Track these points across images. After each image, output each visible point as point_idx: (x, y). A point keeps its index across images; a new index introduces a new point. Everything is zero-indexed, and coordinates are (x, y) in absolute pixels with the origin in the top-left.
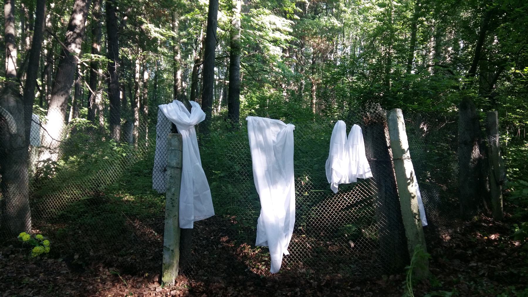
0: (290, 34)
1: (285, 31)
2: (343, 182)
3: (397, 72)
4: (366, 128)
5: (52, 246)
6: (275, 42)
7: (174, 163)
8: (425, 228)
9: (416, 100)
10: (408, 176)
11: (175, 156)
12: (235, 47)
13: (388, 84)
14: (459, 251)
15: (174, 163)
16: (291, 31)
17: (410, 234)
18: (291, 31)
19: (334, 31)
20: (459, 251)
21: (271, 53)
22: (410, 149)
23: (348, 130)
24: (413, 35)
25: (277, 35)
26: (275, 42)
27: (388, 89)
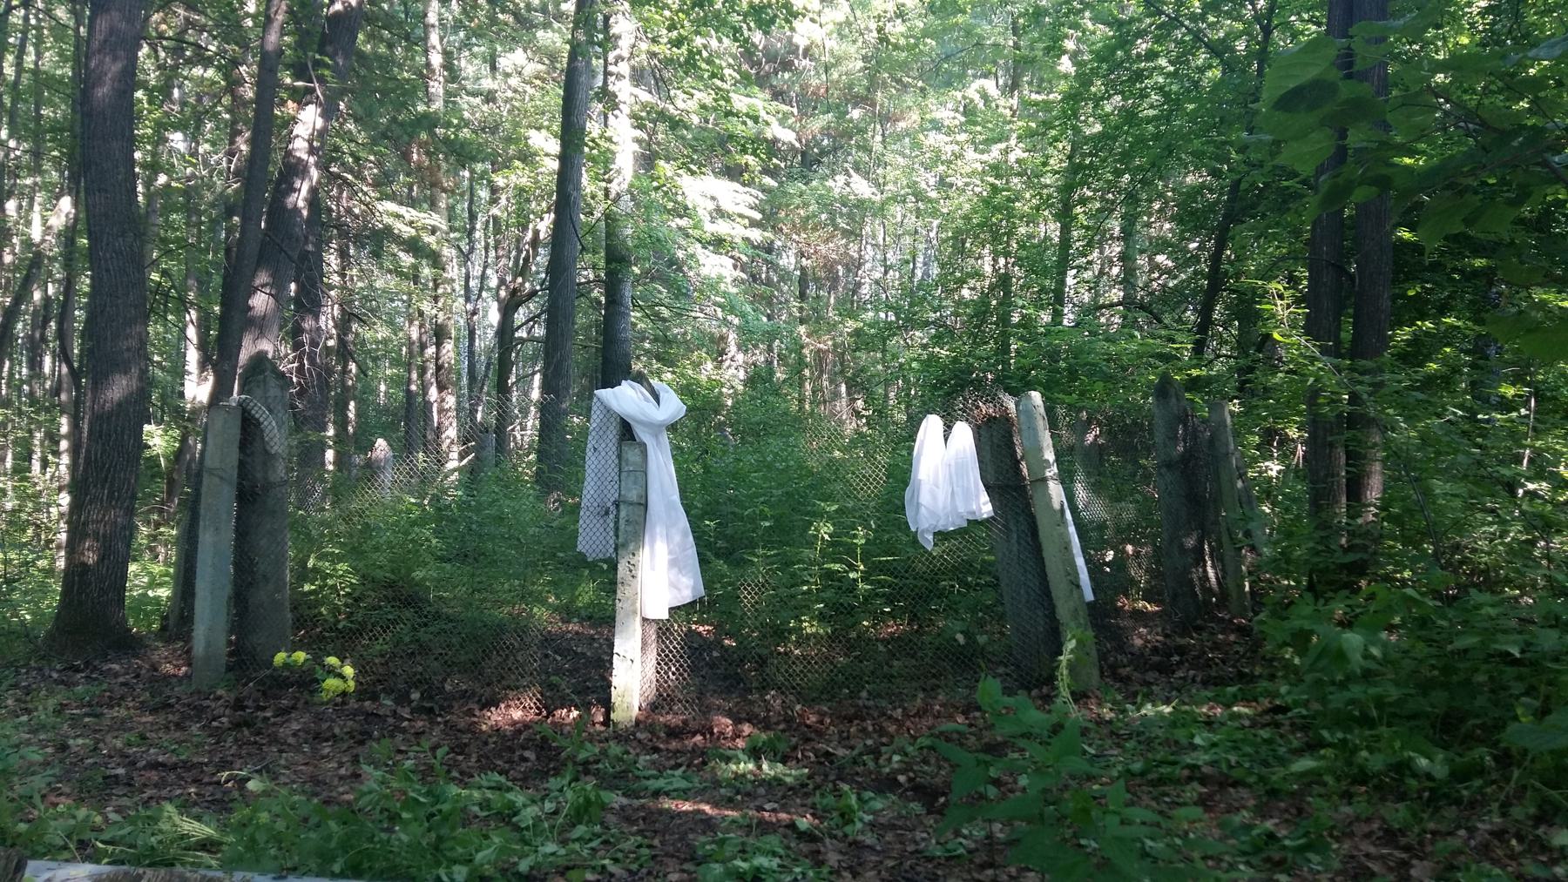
0: (754, 224)
1: (741, 216)
2: (940, 528)
3: (1027, 322)
4: (979, 427)
5: (361, 671)
6: (718, 243)
7: (633, 495)
8: (1089, 604)
9: (1064, 374)
10: (1057, 506)
11: (635, 483)
12: (617, 259)
13: (1005, 348)
14: (1156, 659)
15: (633, 495)
16: (758, 216)
17: (1063, 611)
18: (758, 216)
19: (859, 209)
20: (1156, 659)
21: (704, 271)
22: (1057, 460)
23: (948, 428)
24: (1066, 230)
25: (722, 228)
26: (718, 243)
27: (1006, 363)
